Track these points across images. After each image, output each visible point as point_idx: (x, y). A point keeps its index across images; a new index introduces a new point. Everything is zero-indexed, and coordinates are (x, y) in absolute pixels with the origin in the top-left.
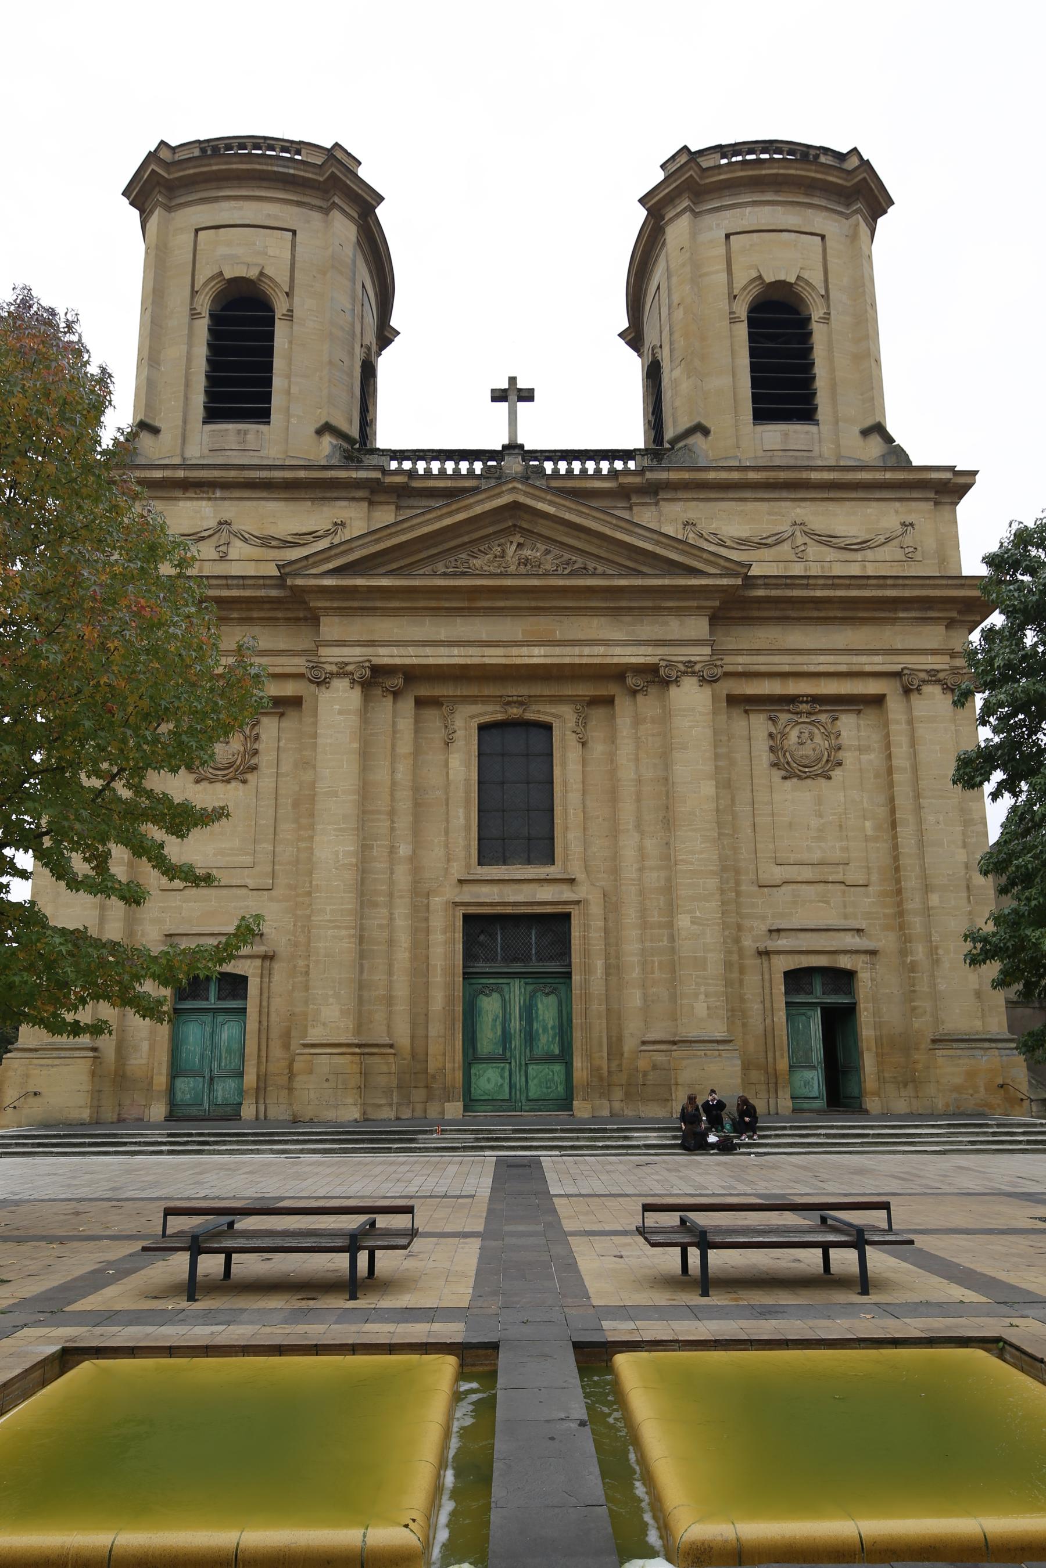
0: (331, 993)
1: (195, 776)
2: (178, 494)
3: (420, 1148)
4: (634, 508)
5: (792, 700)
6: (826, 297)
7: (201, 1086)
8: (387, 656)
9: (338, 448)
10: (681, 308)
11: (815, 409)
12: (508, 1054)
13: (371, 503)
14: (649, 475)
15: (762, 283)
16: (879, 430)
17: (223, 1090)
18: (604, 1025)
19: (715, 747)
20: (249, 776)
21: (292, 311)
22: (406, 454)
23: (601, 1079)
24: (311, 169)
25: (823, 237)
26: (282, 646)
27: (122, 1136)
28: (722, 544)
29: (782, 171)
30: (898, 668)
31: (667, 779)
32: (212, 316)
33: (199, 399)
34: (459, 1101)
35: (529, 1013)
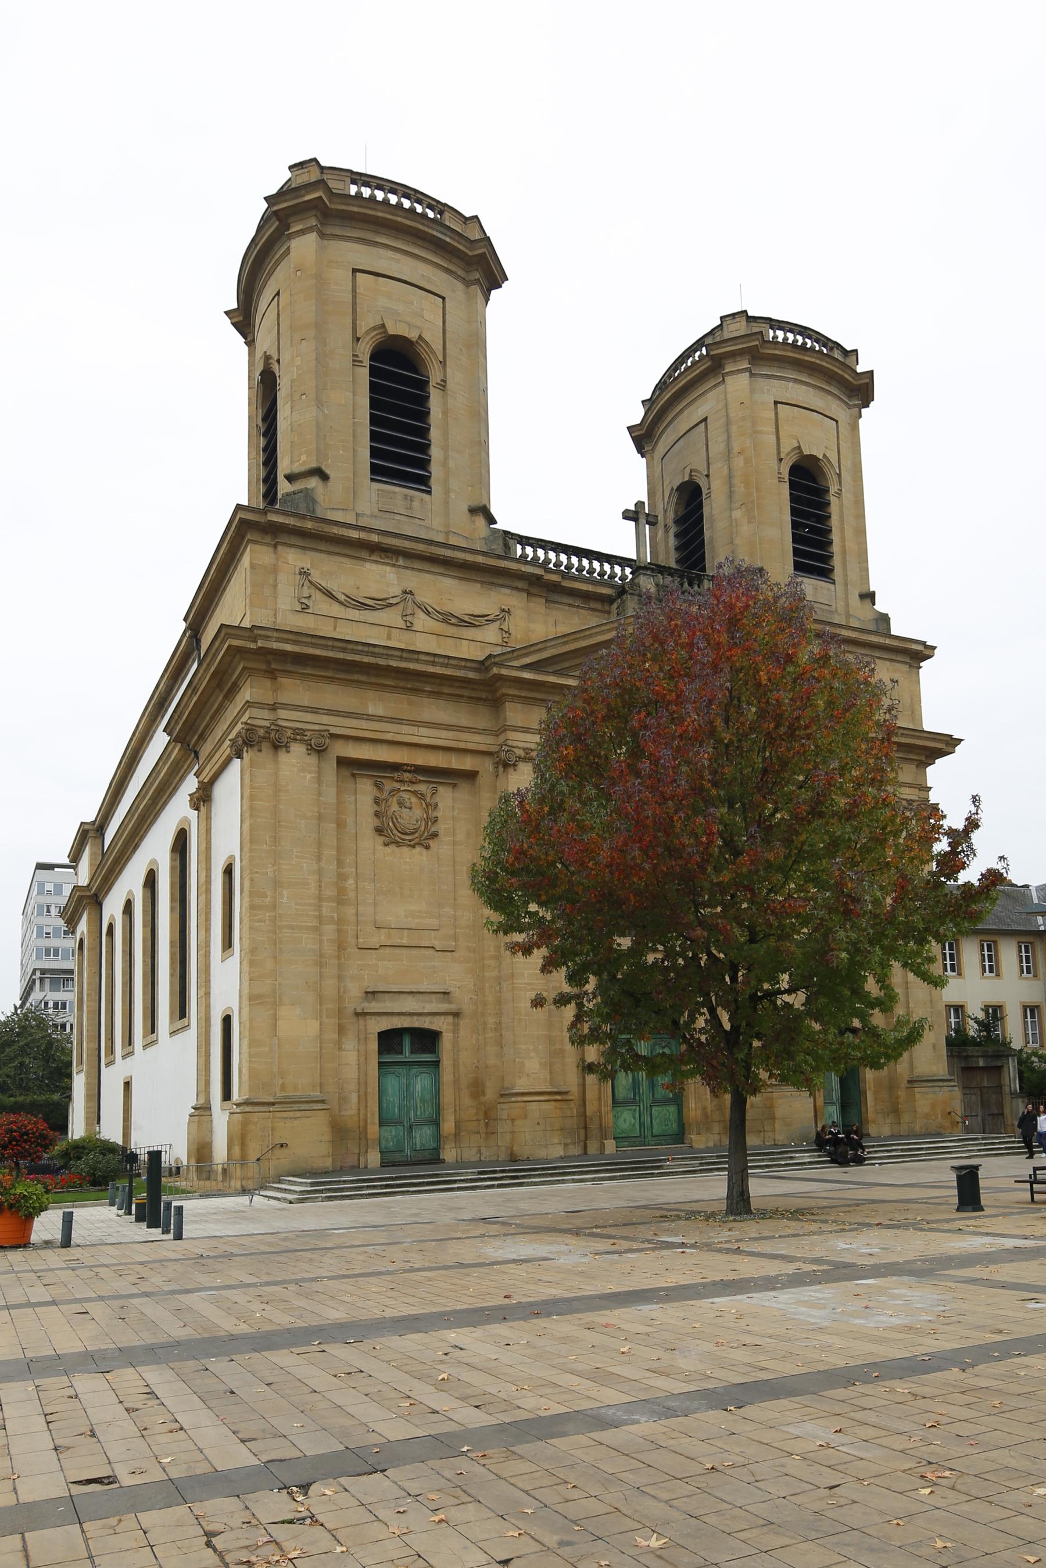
0: (532, 1048)
1: (383, 838)
2: (365, 554)
3: (672, 1172)
7: (402, 1133)
11: (832, 570)
12: (637, 1098)
15: (384, 332)
17: (421, 1136)
20: (431, 842)
21: (445, 381)
24: (463, 242)
25: (444, 298)
26: (464, 723)
27: (442, 1175)
29: (818, 361)
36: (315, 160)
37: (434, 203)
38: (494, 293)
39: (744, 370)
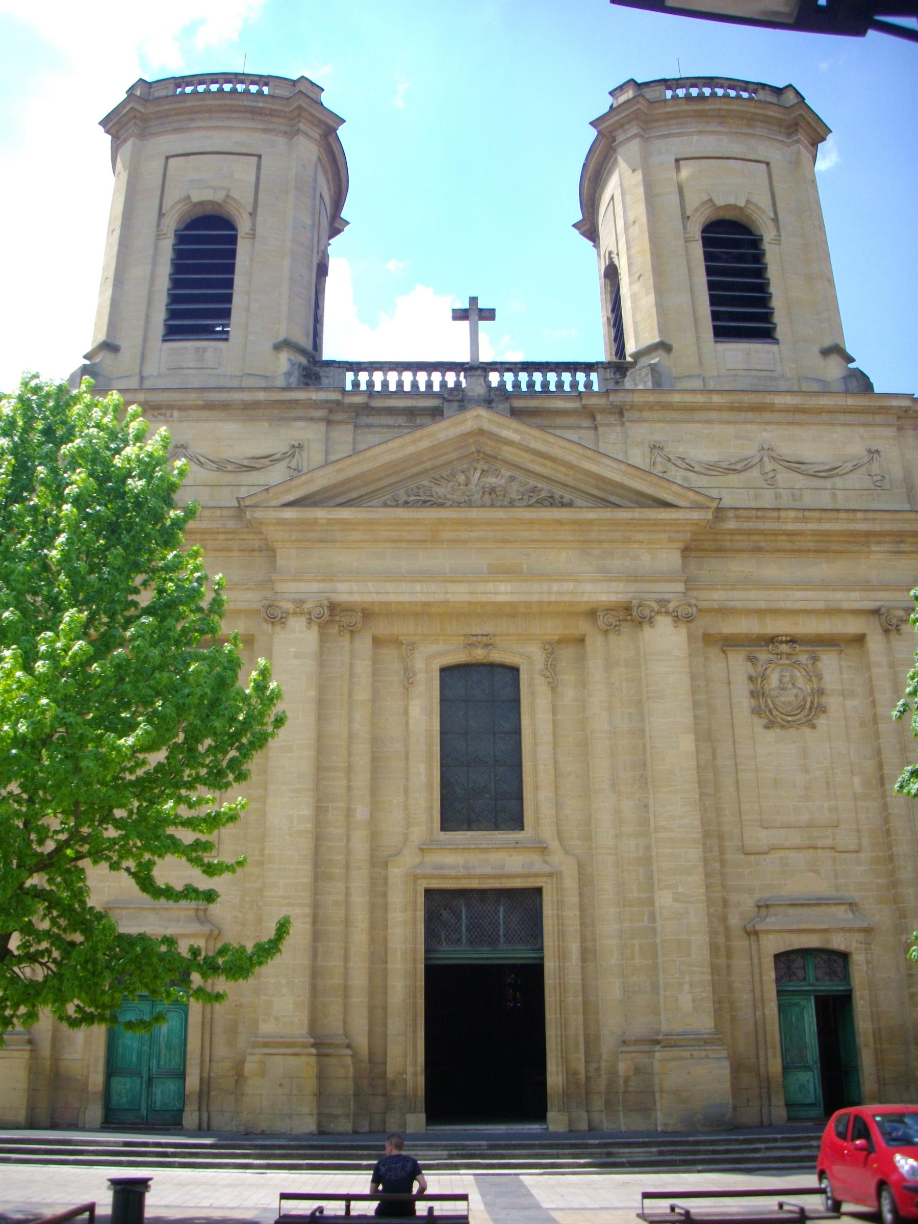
4: (601, 429)
5: (771, 640)
6: (776, 220)
7: (138, 1087)
9: (296, 367)
10: (637, 226)
13: (329, 422)
14: (612, 398)
16: (837, 351)
18: (581, 1021)
19: (693, 693)
22: (363, 366)
23: (578, 1085)
25: (768, 164)
28: (690, 468)
30: (876, 604)
31: (643, 731)
33: (160, 316)
34: (421, 1112)
36: (303, 77)
37: (695, 81)
39: (635, 136)
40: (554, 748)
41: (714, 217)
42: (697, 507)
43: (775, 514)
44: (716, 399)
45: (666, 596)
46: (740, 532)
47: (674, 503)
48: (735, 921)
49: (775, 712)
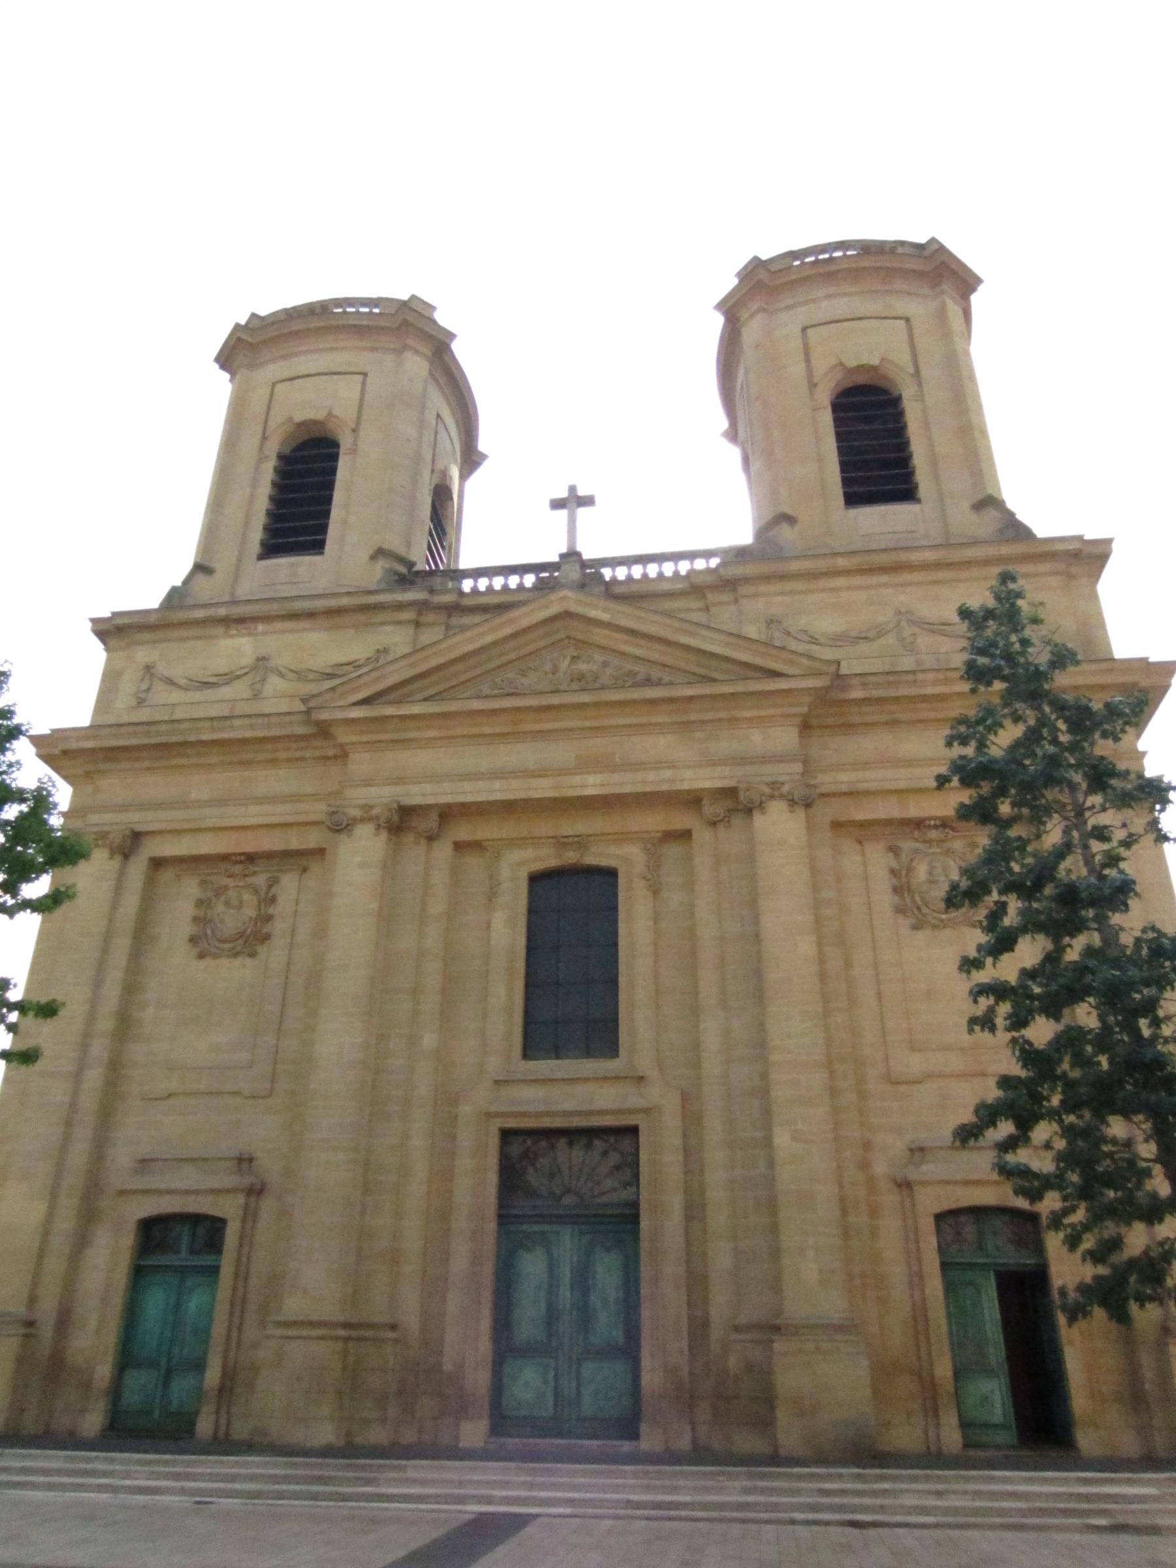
5: (919, 824)
8: (416, 795)
13: (417, 624)
16: (990, 503)
25: (907, 320)
28: (814, 641)
32: (281, 457)
33: (256, 535)
35: (583, 1280)
38: (974, 298)
40: (656, 961)
41: (848, 384)
42: (818, 674)
43: (910, 677)
44: (841, 562)
45: (781, 779)
46: (868, 701)
47: (785, 672)
48: (880, 1168)
49: (925, 910)
